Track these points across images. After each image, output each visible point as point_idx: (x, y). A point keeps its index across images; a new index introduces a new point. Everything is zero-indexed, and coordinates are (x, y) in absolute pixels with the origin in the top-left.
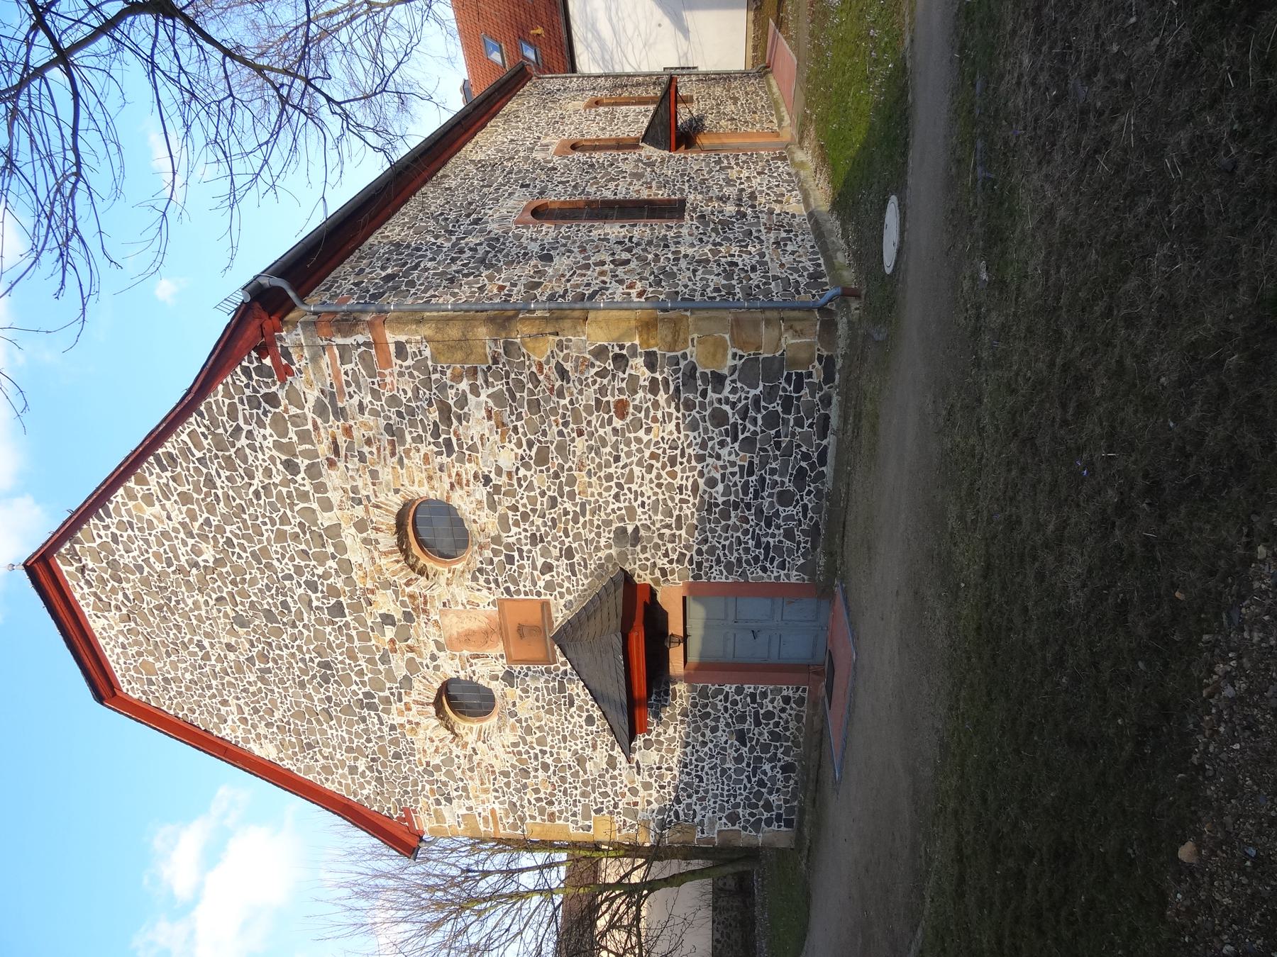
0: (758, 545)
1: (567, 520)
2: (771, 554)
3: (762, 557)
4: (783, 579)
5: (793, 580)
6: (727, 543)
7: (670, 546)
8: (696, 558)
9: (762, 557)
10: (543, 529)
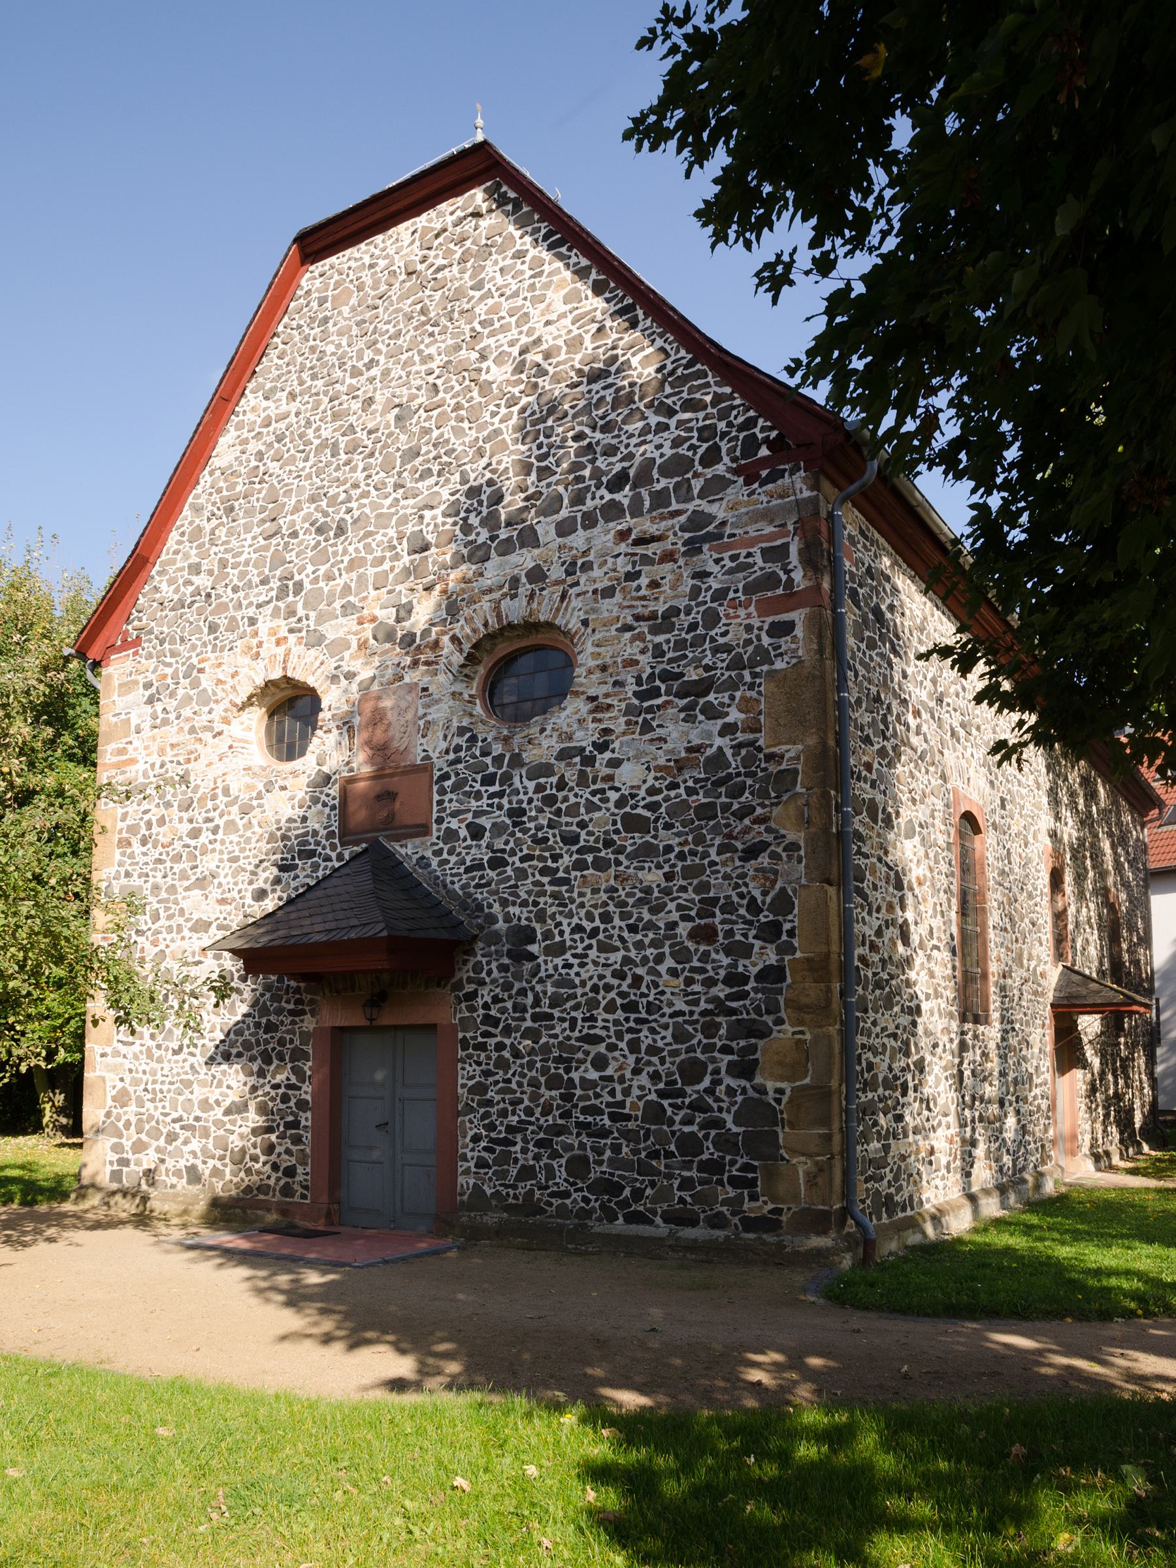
0: (510, 1129)
1: (544, 859)
2: (498, 1148)
3: (493, 1135)
4: (462, 1166)
5: (461, 1180)
6: (514, 1086)
7: (509, 1005)
8: (492, 1042)
9: (493, 1135)
10: (532, 825)
